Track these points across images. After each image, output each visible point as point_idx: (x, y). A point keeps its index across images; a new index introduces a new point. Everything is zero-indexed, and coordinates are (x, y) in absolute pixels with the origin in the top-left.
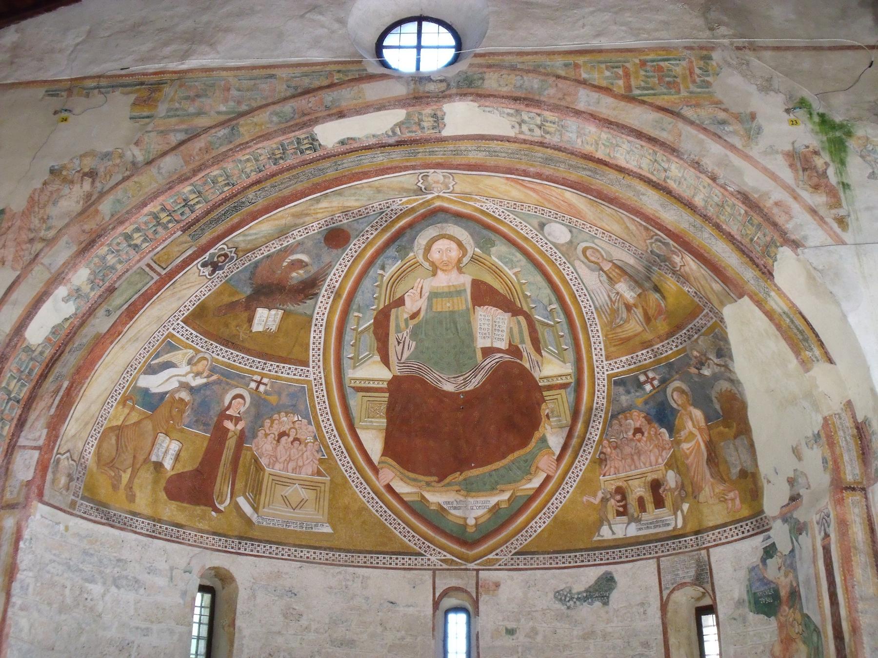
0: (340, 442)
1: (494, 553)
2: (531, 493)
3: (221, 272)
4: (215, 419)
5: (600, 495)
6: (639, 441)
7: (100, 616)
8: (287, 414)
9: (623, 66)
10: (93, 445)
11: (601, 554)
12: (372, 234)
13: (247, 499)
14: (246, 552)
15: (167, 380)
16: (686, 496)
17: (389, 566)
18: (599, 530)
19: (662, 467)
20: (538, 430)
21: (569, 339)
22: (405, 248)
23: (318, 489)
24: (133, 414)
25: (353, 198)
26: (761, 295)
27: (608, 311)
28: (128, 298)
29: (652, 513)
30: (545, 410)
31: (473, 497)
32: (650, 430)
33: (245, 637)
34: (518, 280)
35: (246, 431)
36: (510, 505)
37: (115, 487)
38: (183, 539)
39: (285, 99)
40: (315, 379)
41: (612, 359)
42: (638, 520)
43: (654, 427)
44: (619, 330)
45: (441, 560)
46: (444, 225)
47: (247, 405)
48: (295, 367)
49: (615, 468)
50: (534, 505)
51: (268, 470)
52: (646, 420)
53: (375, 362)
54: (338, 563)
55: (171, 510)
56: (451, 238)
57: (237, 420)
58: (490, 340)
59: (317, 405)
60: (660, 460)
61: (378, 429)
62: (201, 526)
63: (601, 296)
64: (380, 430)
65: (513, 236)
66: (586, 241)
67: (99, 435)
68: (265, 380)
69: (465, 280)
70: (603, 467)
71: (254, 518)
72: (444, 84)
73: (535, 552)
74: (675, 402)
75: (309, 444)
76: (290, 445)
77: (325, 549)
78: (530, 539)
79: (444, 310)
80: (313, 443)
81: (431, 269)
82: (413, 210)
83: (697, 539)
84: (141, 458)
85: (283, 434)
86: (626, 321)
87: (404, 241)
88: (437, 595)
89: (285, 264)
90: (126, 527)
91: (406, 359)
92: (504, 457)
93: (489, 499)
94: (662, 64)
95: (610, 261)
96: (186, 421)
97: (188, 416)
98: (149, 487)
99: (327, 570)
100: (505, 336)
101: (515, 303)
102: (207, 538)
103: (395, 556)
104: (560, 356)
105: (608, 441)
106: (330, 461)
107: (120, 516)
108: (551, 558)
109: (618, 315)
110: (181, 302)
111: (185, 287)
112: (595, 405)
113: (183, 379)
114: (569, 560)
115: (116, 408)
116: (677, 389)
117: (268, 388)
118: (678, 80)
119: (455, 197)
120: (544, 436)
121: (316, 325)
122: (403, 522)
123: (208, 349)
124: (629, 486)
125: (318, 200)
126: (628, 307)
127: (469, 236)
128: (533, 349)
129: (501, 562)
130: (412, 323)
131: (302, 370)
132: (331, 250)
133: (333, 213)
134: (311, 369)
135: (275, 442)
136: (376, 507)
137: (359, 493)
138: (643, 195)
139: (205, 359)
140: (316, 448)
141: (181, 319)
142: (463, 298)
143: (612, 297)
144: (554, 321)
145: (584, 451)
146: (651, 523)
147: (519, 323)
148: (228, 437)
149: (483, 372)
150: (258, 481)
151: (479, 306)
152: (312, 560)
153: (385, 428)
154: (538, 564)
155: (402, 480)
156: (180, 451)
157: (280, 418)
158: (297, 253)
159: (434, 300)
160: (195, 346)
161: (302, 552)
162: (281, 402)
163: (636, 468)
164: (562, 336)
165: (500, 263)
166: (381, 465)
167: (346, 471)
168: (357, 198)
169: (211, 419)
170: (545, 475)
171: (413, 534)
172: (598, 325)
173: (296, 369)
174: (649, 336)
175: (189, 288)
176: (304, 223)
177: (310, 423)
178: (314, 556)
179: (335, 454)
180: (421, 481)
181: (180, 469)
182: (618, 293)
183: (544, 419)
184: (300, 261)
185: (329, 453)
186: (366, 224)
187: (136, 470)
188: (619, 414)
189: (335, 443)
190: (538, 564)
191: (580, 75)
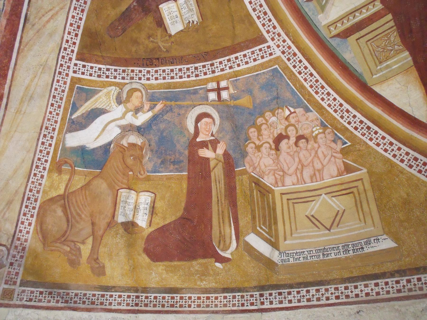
0: (358, 115)
4: (186, 152)
8: (273, 112)
13: (259, 234)
14: (273, 306)
15: (104, 129)
23: (355, 190)
24: (76, 178)
35: (231, 152)
38: (181, 306)
40: (283, 53)
47: (218, 121)
51: (278, 190)
59: (305, 84)
61: (405, 71)
62: (204, 284)
64: (407, 70)
68: (223, 84)
71: (276, 257)
75: (319, 136)
76: (295, 148)
77: (392, 275)
80: (324, 133)
84: (102, 223)
90: (94, 306)
96: (150, 166)
97: (150, 160)
98: (123, 253)
99: (403, 309)
102: (216, 298)
107: (85, 295)
110: (58, 38)
111: (45, 19)
113: (123, 122)
115: (49, 177)
117: (232, 91)
123: (132, 78)
134: (271, 43)
135: (273, 152)
137: (419, 175)
139: (136, 90)
140: (330, 137)
148: (211, 169)
150: (269, 207)
152: (375, 297)
153: (412, 63)
156: (154, 202)
160: (113, 80)
161: (356, 287)
162: (258, 101)
167: (386, 150)
169: (181, 154)
173: (253, 53)
175: (52, 17)
177: (307, 110)
178: (377, 289)
179: (359, 135)
181: (159, 222)
185: (353, 138)
187: (99, 238)
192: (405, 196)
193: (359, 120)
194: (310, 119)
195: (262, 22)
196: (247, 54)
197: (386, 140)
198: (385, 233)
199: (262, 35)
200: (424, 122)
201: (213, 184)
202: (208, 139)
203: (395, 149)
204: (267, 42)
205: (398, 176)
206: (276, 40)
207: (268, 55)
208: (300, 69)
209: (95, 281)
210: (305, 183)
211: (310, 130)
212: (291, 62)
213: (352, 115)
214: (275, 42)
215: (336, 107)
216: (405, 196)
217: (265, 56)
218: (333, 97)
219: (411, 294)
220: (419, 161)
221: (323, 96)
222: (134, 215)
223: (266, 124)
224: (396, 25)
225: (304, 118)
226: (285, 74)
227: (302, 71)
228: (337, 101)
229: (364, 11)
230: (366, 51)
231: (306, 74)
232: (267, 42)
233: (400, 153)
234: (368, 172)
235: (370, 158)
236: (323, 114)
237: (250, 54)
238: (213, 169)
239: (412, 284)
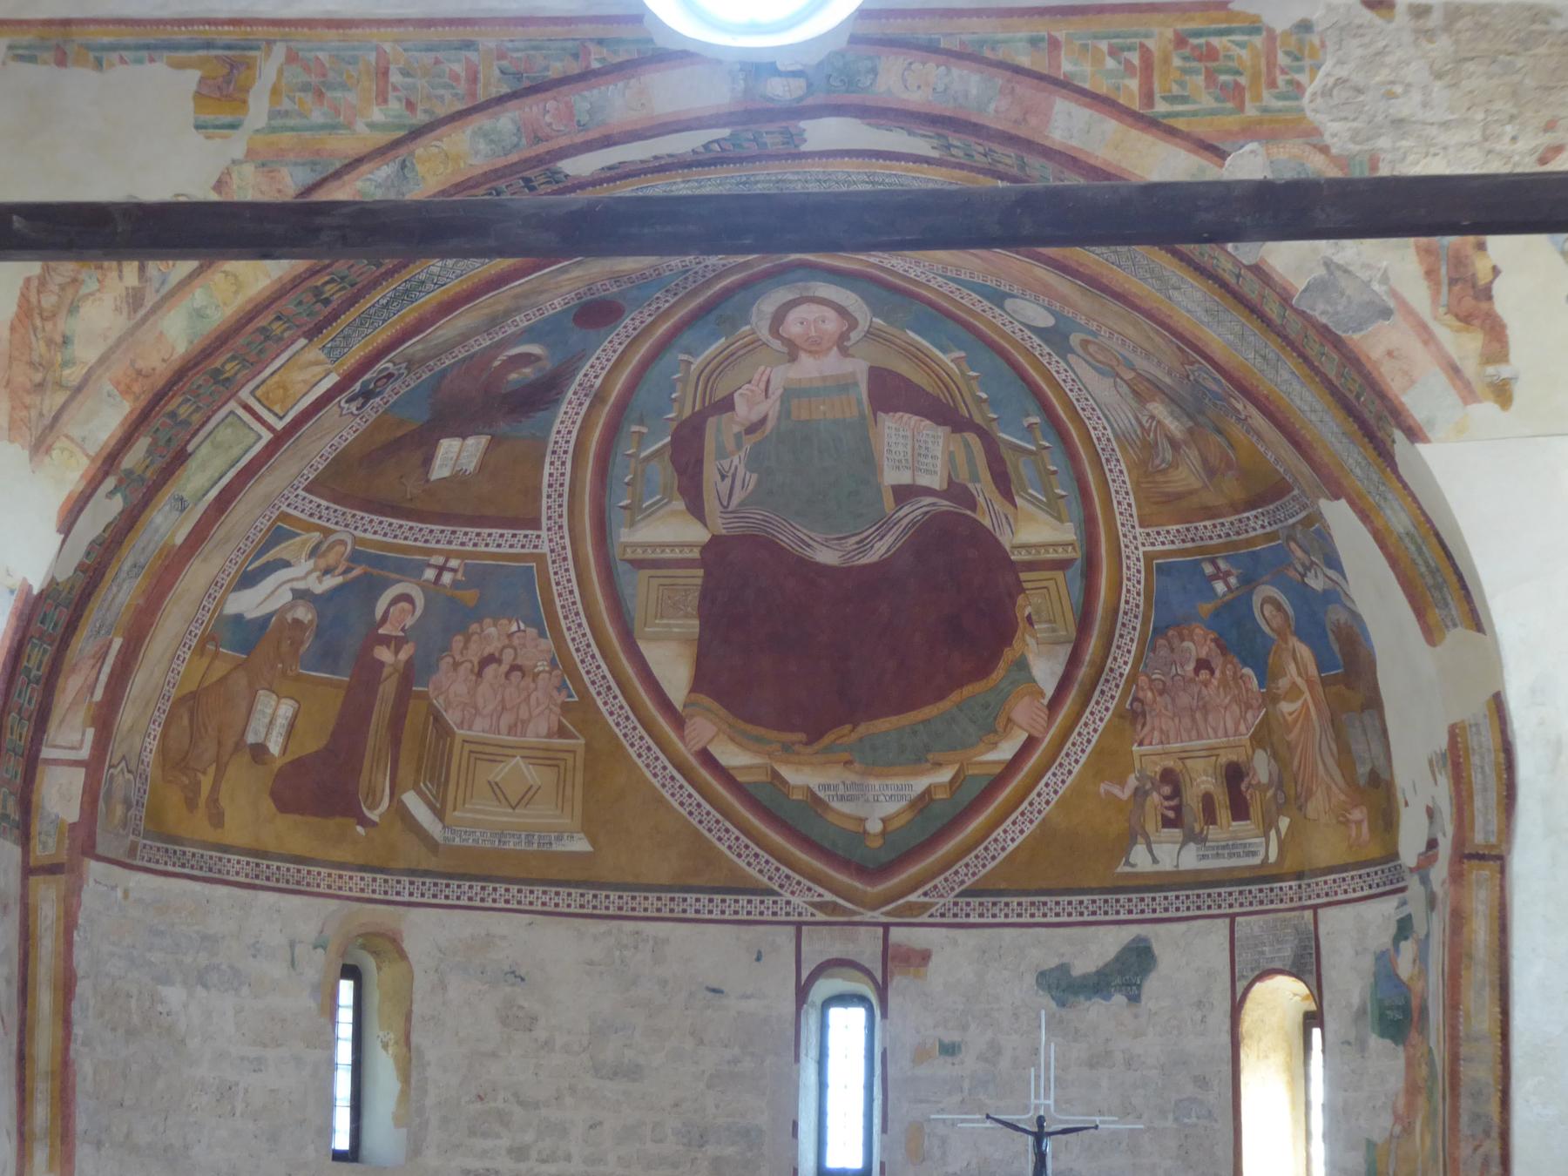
1: (920, 891)
2: (997, 770)
3: (378, 399)
5: (1132, 782)
6: (1206, 684)
7: (183, 1041)
9: (1142, 46)
10: (155, 736)
11: (1130, 900)
13: (420, 793)
14: (425, 900)
16: (1285, 802)
18: (1128, 854)
19: (1245, 739)
20: (1010, 645)
23: (562, 764)
26: (1370, 499)
28: (217, 475)
29: (1226, 829)
32: (1224, 666)
33: (429, 1064)
36: (953, 793)
37: (191, 804)
39: (501, 100)
40: (552, 551)
42: (1200, 839)
43: (1231, 663)
44: (1160, 478)
45: (813, 905)
47: (418, 612)
49: (1162, 731)
52: (1218, 646)
53: (674, 513)
55: (293, 833)
57: (396, 643)
60: (1242, 728)
62: (338, 855)
67: (164, 717)
68: (454, 563)
69: (857, 368)
70: (1139, 727)
72: (802, 82)
74: (1268, 624)
75: (541, 676)
76: (503, 680)
78: (993, 864)
81: (785, 350)
83: (1300, 887)
85: (490, 660)
86: (1174, 465)
88: (805, 975)
89: (497, 363)
93: (912, 781)
94: (1216, 41)
101: (956, 410)
102: (351, 878)
104: (1053, 507)
105: (1148, 676)
109: (1158, 455)
112: (1122, 605)
113: (301, 585)
114: (1069, 909)
116: (1269, 600)
117: (459, 576)
118: (1243, 80)
122: (736, 826)
124: (1187, 770)
125: (564, 270)
126: (1174, 445)
129: (933, 910)
131: (526, 536)
135: (474, 678)
136: (680, 797)
138: (1175, 288)
139: (343, 543)
141: (302, 486)
143: (1144, 422)
145: (1103, 692)
146: (1224, 847)
147: (967, 445)
149: (896, 531)
151: (886, 411)
153: (697, 636)
155: (732, 740)
156: (295, 716)
157: (482, 631)
163: (1200, 737)
164: (1054, 473)
167: (618, 724)
170: (1025, 736)
171: (757, 850)
174: (1210, 499)
183: (1022, 624)
184: (529, 355)
185: (584, 693)
188: (1167, 627)
189: (593, 670)
191: (1059, 67)
198: (583, 830)
201: (378, 703)
202: (394, 634)
209: (211, 835)
210: (499, 734)
219: (595, 912)
222: (267, 735)
223: (479, 634)
224: (702, 586)
238: (385, 680)
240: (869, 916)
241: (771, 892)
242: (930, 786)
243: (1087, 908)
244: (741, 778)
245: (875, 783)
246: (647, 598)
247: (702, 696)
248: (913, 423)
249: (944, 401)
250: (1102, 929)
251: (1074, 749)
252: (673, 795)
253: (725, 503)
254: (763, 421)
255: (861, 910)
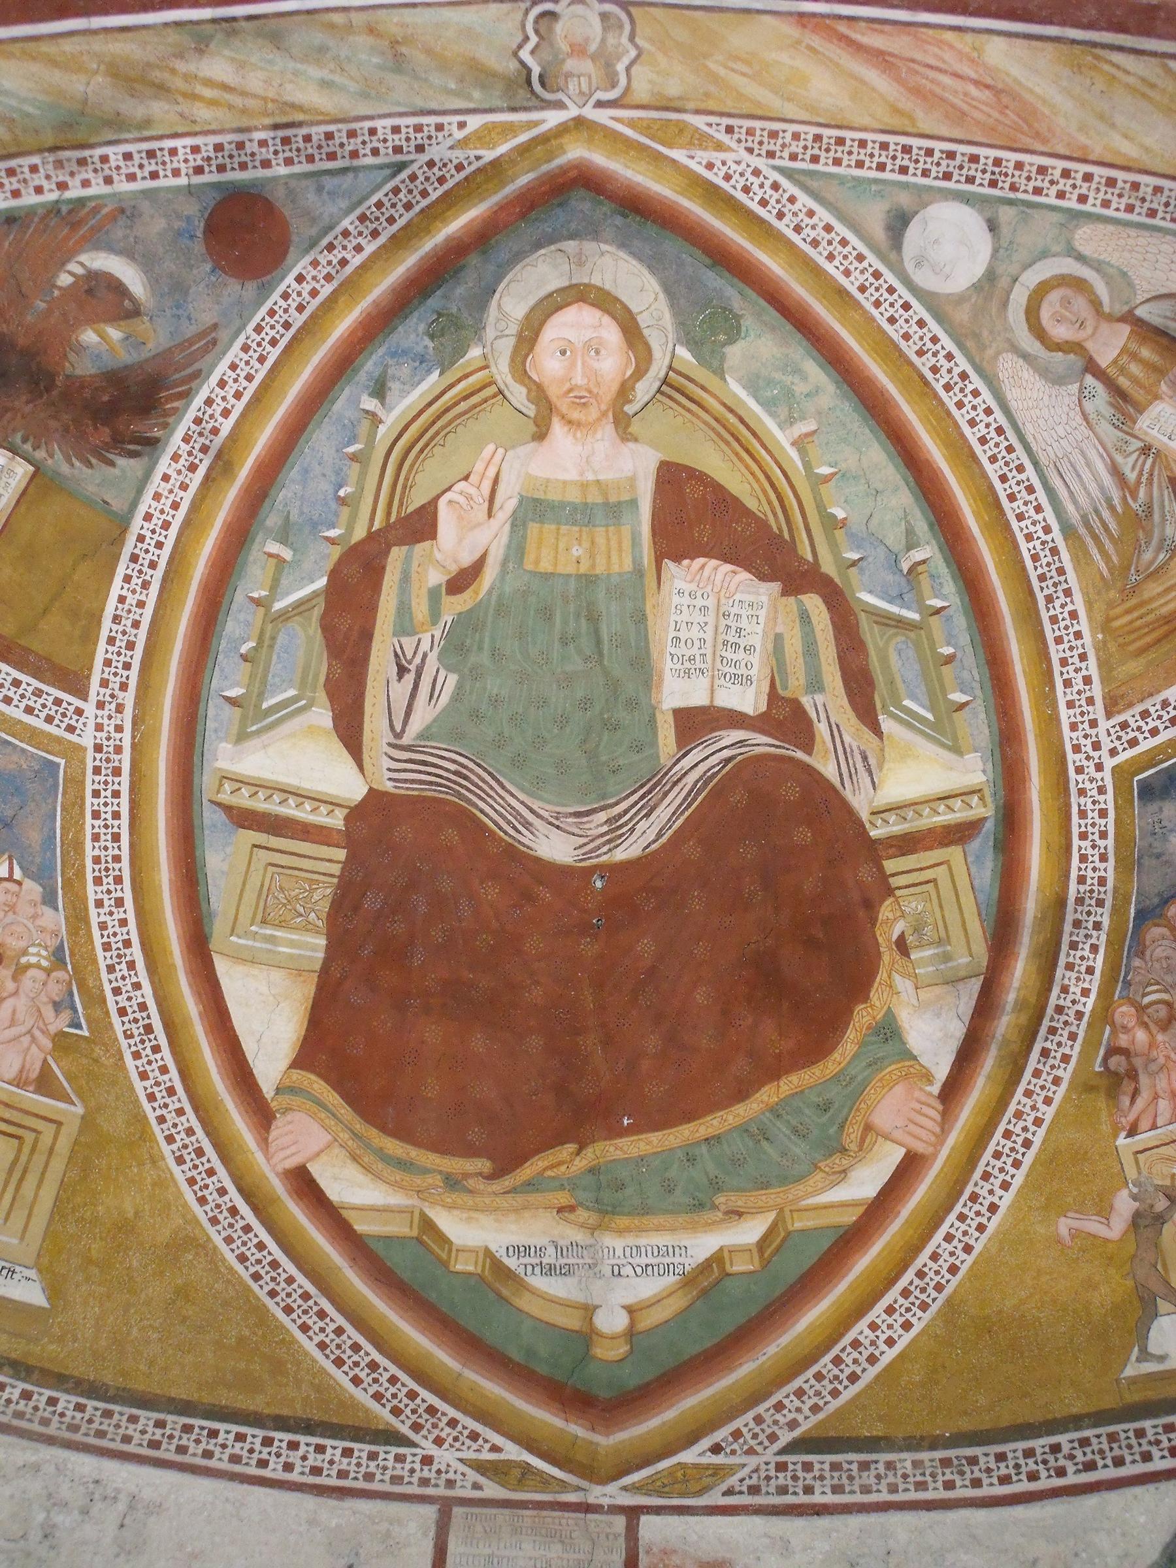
1: (706, 1443)
2: (849, 1218)
5: (1124, 1205)
12: (359, 249)
17: (253, 1471)
18: (1143, 1338)
20: (866, 999)
21: (971, 667)
22: (455, 323)
23: (29, 1137)
25: (315, 72)
27: (1113, 526)
30: (891, 923)
31: (621, 1232)
34: (807, 465)
36: (766, 1264)
40: (98, 748)
41: (1131, 705)
44: (1153, 589)
45: (480, 1467)
46: (589, 246)
48: (36, 683)
50: (863, 1263)
53: (312, 730)
54: (36, 1427)
56: (604, 301)
58: (703, 682)
63: (1086, 475)
64: (300, 972)
65: (800, 290)
66: (1044, 255)
70: (1126, 1101)
73: (877, 1440)
75: (32, 972)
79: (561, 569)
80: (48, 972)
81: (531, 410)
82: (495, 171)
87: (461, 290)
89: (65, 280)
91: (421, 736)
92: (741, 1094)
93: (685, 1239)
95: (1122, 319)
100: (757, 667)
103: (287, 1437)
106: (98, 1051)
108: (946, 1463)
109: (1149, 535)
112: (1073, 886)
119: (631, 124)
120: (890, 1016)
121: (134, 558)
127: (662, 296)
128: (851, 713)
129: (733, 1481)
130: (454, 606)
132: (224, 277)
133: (245, 122)
134: (89, 708)
137: (184, 1187)
140: (55, 990)
142: (626, 530)
144: (921, 607)
147: (805, 618)
149: (676, 797)
151: (677, 559)
153: (318, 967)
154: (893, 1489)
155: (355, 1158)
158: (111, 249)
159: (533, 528)
164: (950, 659)
165: (752, 404)
166: (285, 1100)
168: (324, 74)
170: (898, 1154)
171: (376, 1356)
172: (1078, 596)
173: (38, 693)
176: (147, 123)
177: (49, 899)
179: (119, 1030)
180: (425, 1171)
182: (1146, 450)
184: (118, 288)
185: (101, 1026)
186: (344, 204)
190: (893, 1489)
192: (130, 1215)
193: (140, 1000)
194: (39, 922)
195: (109, 656)
196: (24, 686)
197: (166, 1077)
199: (88, 677)
200: (260, 1091)
203: (171, 1107)
204: (86, 700)
205: (141, 1164)
206: (106, 713)
207: (63, 726)
208: (103, 809)
211: (22, 944)
212: (97, 778)
213: (135, 980)
214: (100, 713)
215: (112, 939)
216: (130, 1215)
217: (56, 722)
218: (122, 916)
220: (204, 1159)
221: (106, 897)
225: (31, 911)
226: (64, 794)
227: (103, 816)
228: (125, 930)
229: (308, 806)
230: (255, 881)
231: (106, 826)
232: (86, 700)
233: (177, 1121)
234: (83, 1117)
235: (108, 1092)
236: (76, 934)
237: (30, 689)
239: (32, 1404)
240: (601, 1494)
241: (392, 1438)
242: (721, 1249)
243: (1071, 1457)
244: (361, 1227)
245: (613, 1242)
246: (244, 884)
247: (313, 1077)
248: (719, 577)
249: (775, 529)
250: (1113, 1498)
251: (999, 1164)
252: (229, 1240)
253: (398, 728)
254: (478, 567)
255: (584, 1484)
